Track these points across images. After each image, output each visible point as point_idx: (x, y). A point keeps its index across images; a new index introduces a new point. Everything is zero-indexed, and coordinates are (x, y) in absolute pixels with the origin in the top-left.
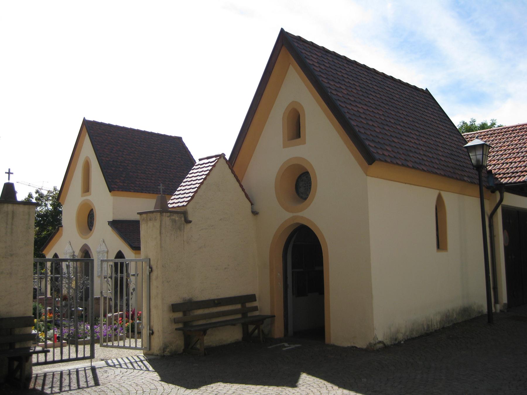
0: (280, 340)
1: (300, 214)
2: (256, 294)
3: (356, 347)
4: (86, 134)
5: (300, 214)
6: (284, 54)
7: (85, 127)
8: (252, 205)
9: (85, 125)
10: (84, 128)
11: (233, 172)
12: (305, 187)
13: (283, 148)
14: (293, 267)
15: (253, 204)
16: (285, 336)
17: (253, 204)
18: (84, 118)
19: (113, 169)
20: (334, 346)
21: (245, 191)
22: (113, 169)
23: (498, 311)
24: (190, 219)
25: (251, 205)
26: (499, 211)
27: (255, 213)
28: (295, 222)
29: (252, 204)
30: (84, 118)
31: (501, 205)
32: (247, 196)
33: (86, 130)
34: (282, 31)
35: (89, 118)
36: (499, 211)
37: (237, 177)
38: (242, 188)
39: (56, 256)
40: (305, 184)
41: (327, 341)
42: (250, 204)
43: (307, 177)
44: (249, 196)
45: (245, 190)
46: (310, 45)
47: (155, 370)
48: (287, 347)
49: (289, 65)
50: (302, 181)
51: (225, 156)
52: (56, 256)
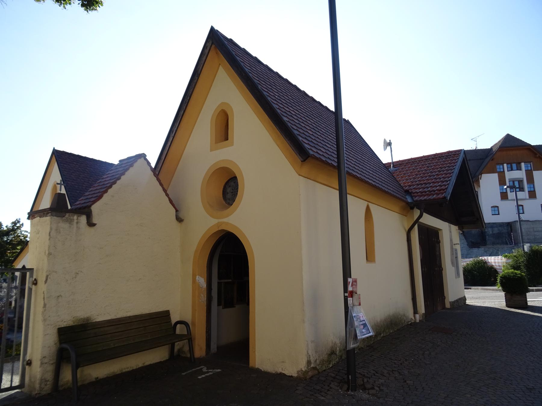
0: (201, 361)
1: (225, 220)
2: (170, 310)
3: (284, 375)
4: (55, 162)
5: (225, 220)
6: (215, 57)
7: (55, 158)
8: (177, 212)
9: (55, 155)
10: (54, 158)
11: (158, 180)
12: (232, 192)
13: (210, 151)
14: (220, 278)
15: (178, 211)
16: (206, 354)
17: (178, 211)
18: (54, 148)
19: (78, 192)
20: (258, 371)
21: (169, 196)
22: (78, 192)
23: (418, 321)
24: (94, 222)
25: (176, 211)
26: (416, 226)
27: (179, 220)
28: (220, 229)
29: (177, 211)
30: (54, 148)
31: (415, 220)
32: (171, 202)
33: (55, 160)
34: (212, 29)
35: (58, 148)
36: (416, 226)
37: (161, 181)
38: (165, 193)
39: (24, 267)
40: (233, 190)
41: (251, 364)
42: (175, 210)
43: (235, 182)
44: (173, 202)
45: (169, 195)
46: (242, 50)
47: (477, 150)
48: (207, 372)
49: (219, 66)
50: (230, 187)
51: (146, 157)
52: (24, 267)
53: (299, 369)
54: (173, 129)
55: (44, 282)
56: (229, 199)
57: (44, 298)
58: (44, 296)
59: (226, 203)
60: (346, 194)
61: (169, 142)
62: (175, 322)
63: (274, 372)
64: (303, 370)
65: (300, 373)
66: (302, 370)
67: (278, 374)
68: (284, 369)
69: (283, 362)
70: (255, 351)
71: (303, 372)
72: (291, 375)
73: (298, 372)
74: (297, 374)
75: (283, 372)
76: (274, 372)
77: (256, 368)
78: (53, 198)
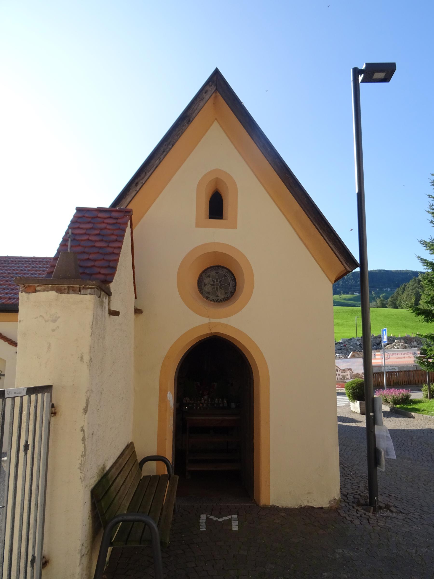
1: (206, 320)
5: (206, 320)
20: (274, 510)
40: (214, 281)
41: (263, 501)
50: (209, 276)
53: (332, 498)
54: (136, 181)
55: (82, 411)
56: (208, 293)
57: (84, 440)
58: (84, 435)
59: (203, 297)
60: (370, 312)
61: (127, 197)
62: (142, 458)
63: (296, 507)
64: (337, 498)
65: (332, 502)
66: (335, 499)
67: (301, 508)
68: (310, 501)
69: (310, 493)
70: (269, 484)
71: (336, 501)
72: (320, 506)
73: (330, 502)
74: (329, 505)
75: (310, 504)
76: (298, 506)
77: (270, 506)
78: (337, 278)
